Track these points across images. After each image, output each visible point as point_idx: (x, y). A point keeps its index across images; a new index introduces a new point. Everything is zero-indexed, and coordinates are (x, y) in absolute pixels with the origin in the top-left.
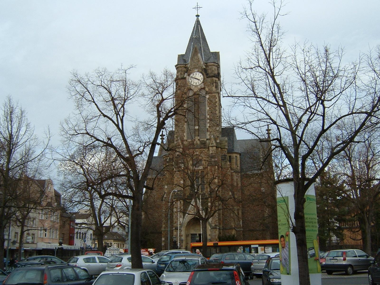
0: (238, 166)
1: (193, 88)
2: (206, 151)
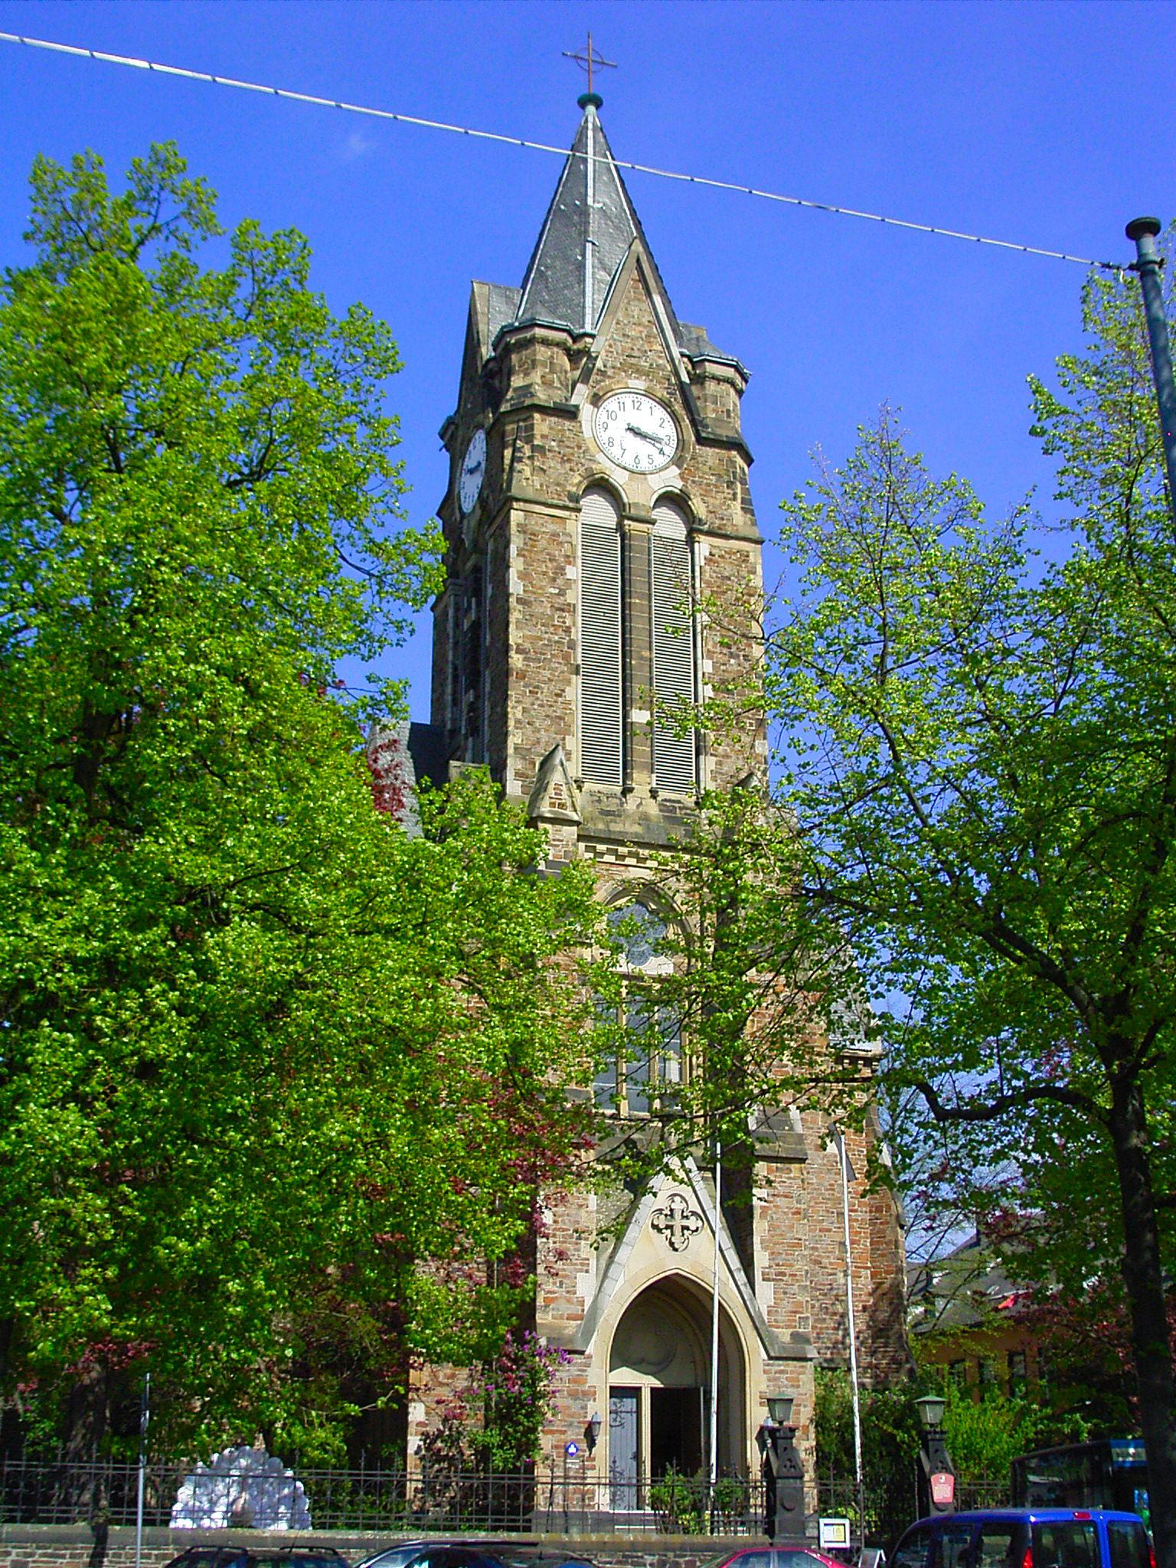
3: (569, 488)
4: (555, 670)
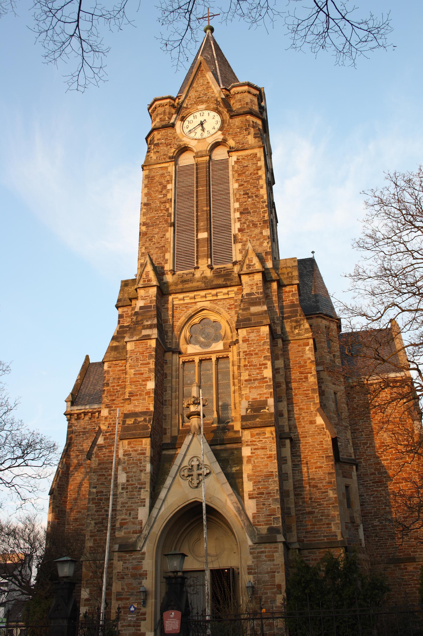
0: (334, 356)
1: (192, 144)
2: (232, 295)
3: (169, 155)
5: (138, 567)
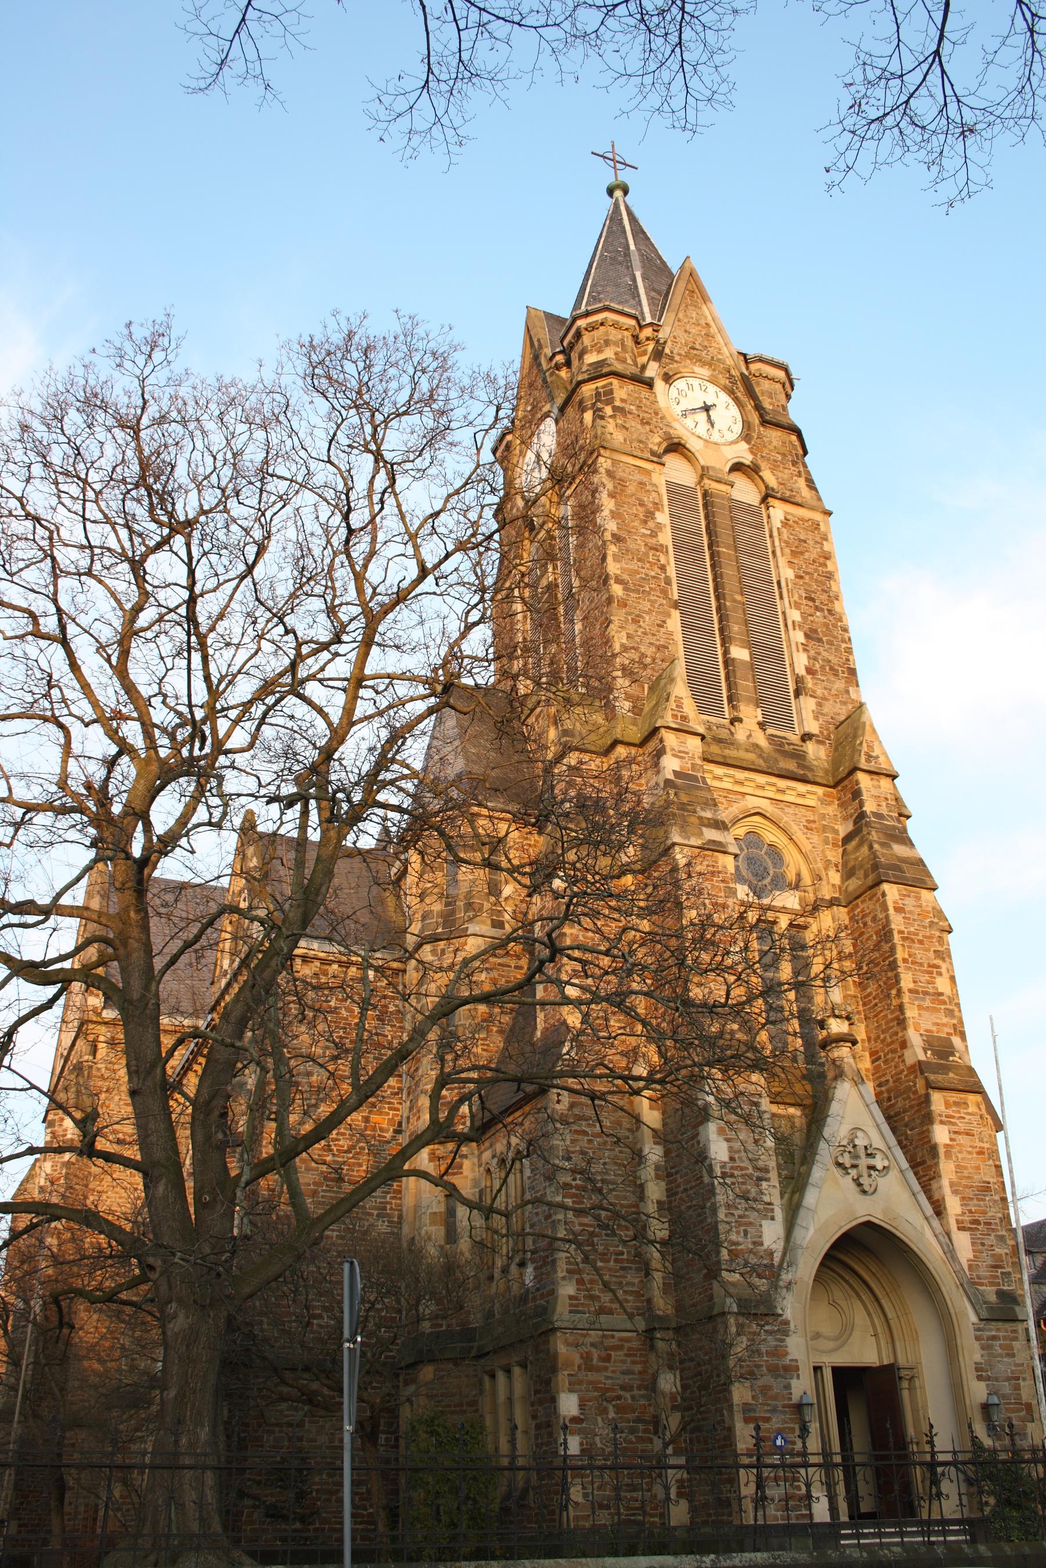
4: (653, 602)
5: (779, 1352)
